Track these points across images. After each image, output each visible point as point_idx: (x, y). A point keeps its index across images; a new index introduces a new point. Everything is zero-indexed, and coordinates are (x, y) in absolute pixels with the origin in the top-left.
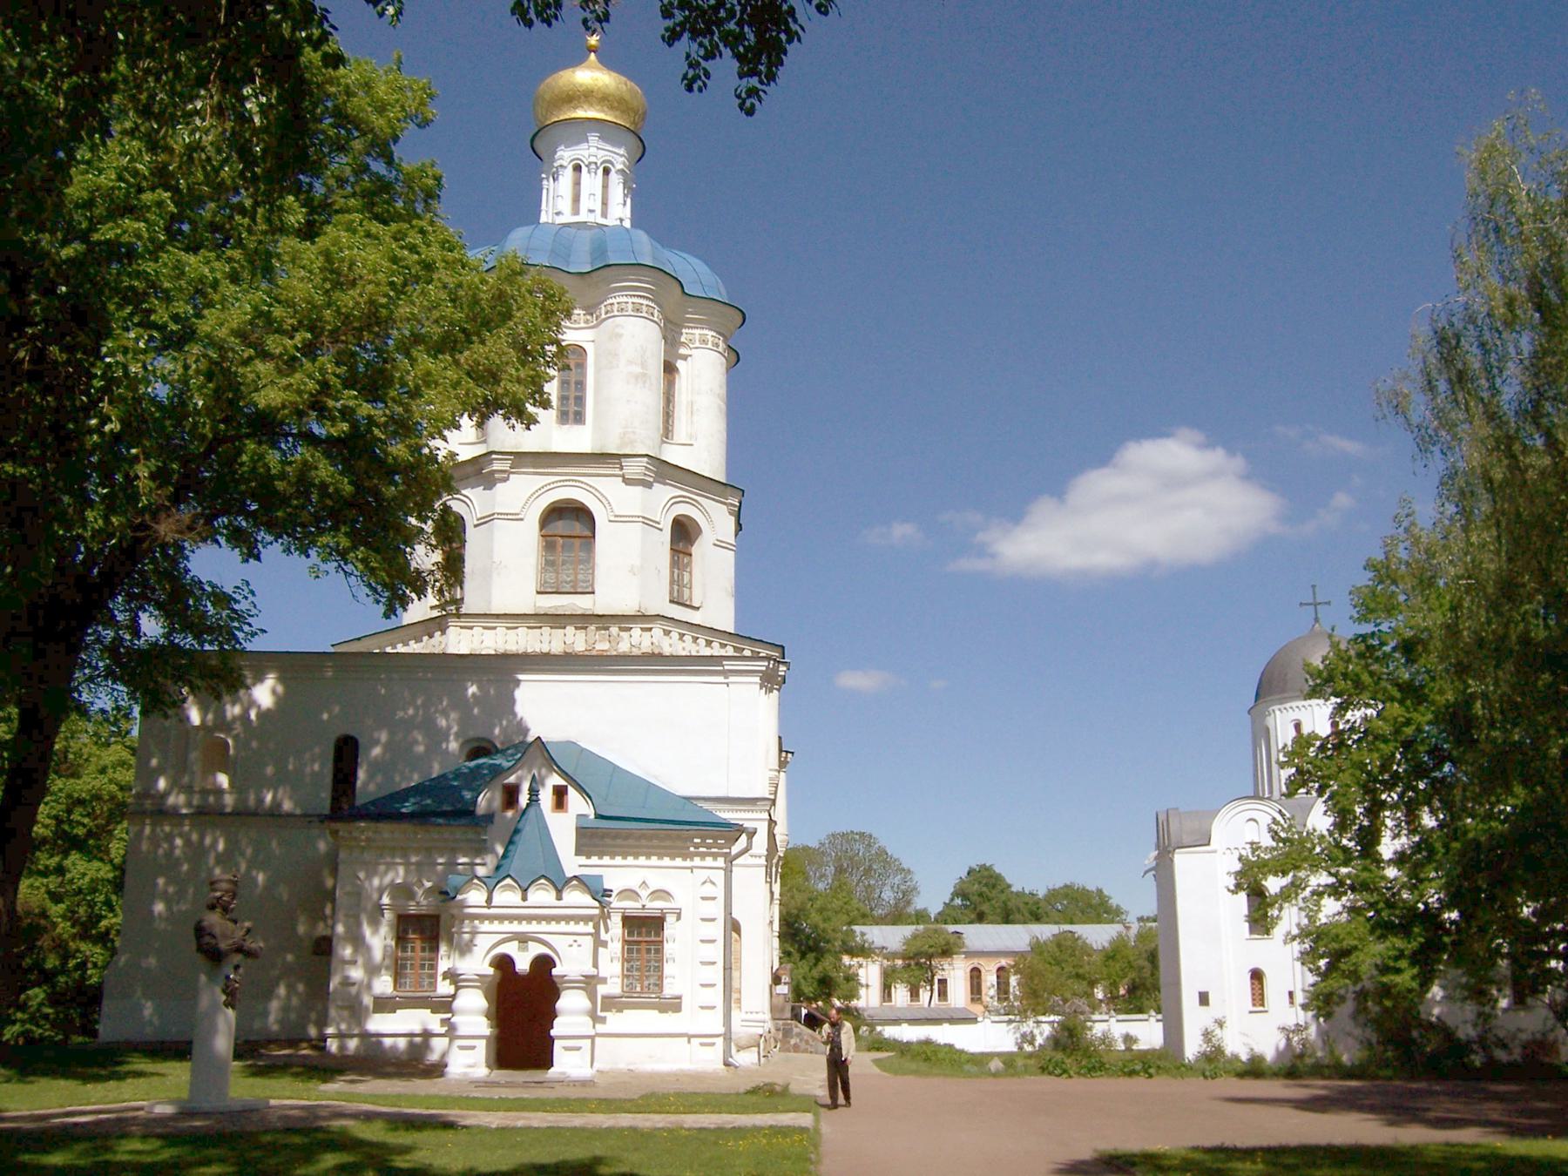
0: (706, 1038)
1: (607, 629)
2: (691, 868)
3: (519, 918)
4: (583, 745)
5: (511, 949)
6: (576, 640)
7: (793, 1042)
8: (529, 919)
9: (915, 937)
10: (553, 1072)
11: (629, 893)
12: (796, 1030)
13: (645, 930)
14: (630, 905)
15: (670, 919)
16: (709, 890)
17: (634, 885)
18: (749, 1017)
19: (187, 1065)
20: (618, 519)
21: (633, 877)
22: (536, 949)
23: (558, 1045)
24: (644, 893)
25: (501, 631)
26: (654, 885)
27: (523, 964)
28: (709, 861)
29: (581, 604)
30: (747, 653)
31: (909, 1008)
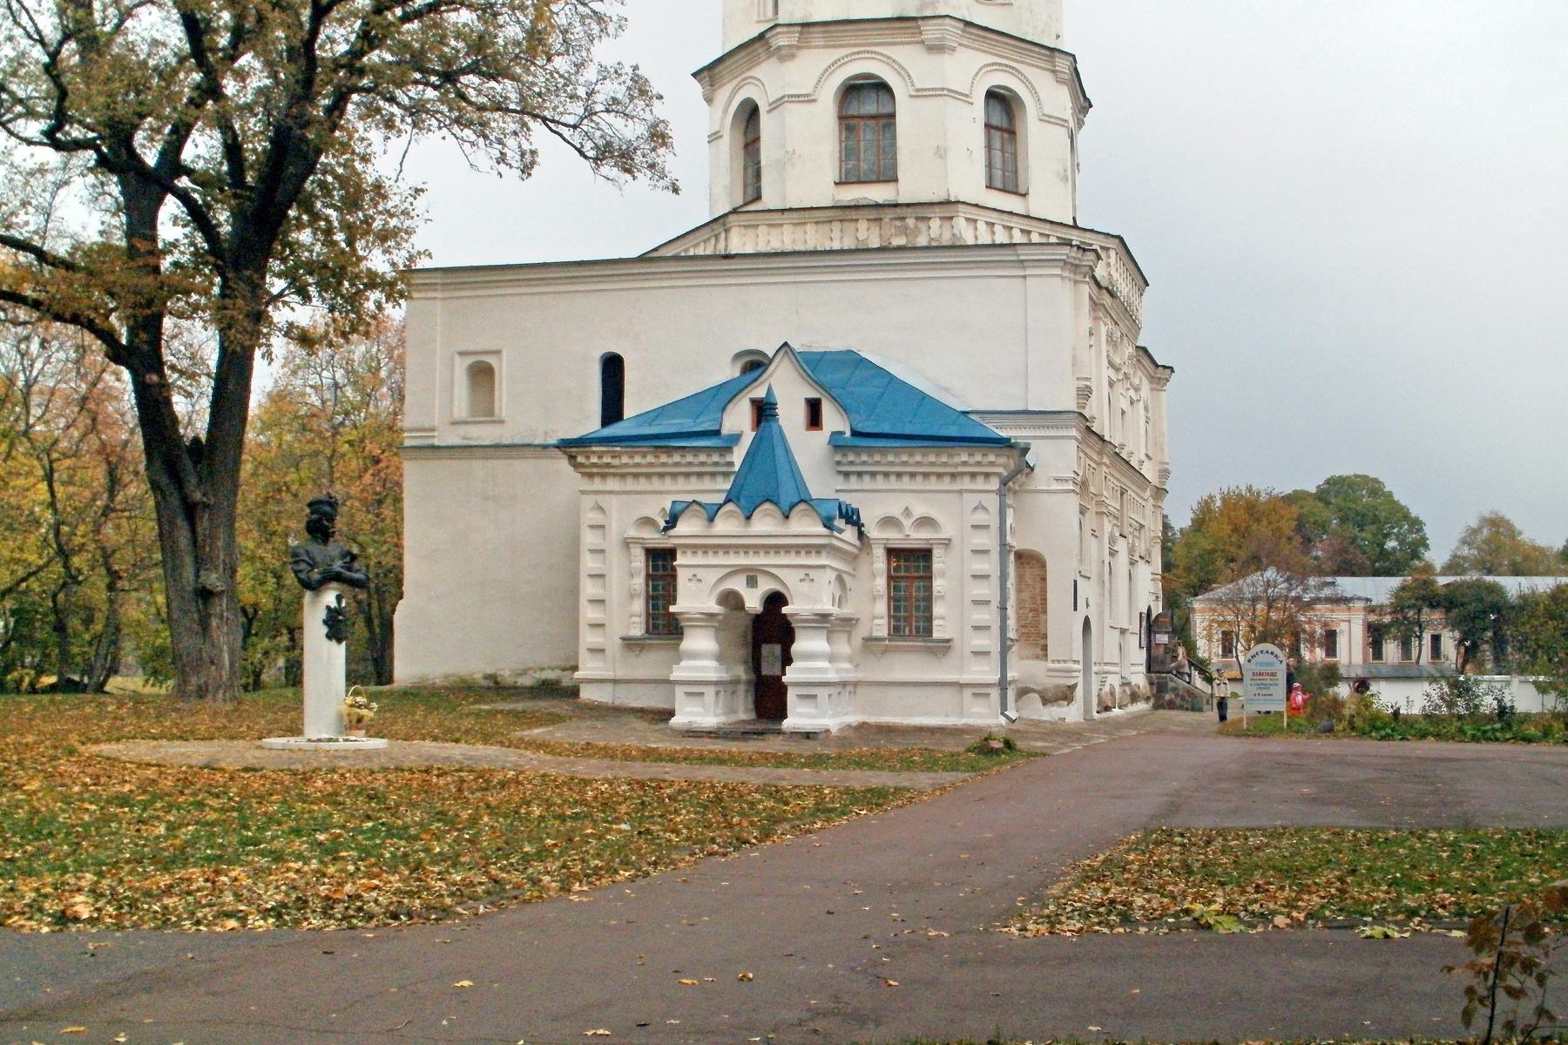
0: (979, 690)
1: (903, 219)
2: (961, 492)
3: (746, 549)
4: (863, 355)
5: (738, 585)
6: (871, 236)
7: (1167, 697)
8: (756, 549)
9: (1403, 588)
10: (788, 724)
11: (889, 522)
12: (1171, 685)
13: (911, 565)
14: (895, 538)
15: (936, 552)
16: (980, 518)
17: (895, 511)
18: (1057, 666)
19: (753, 716)
20: (920, 94)
21: (895, 505)
22: (766, 586)
23: (791, 695)
24: (907, 523)
25: (787, 229)
26: (919, 510)
27: (753, 602)
28: (980, 484)
29: (878, 193)
30: (1035, 238)
31: (1401, 665)
